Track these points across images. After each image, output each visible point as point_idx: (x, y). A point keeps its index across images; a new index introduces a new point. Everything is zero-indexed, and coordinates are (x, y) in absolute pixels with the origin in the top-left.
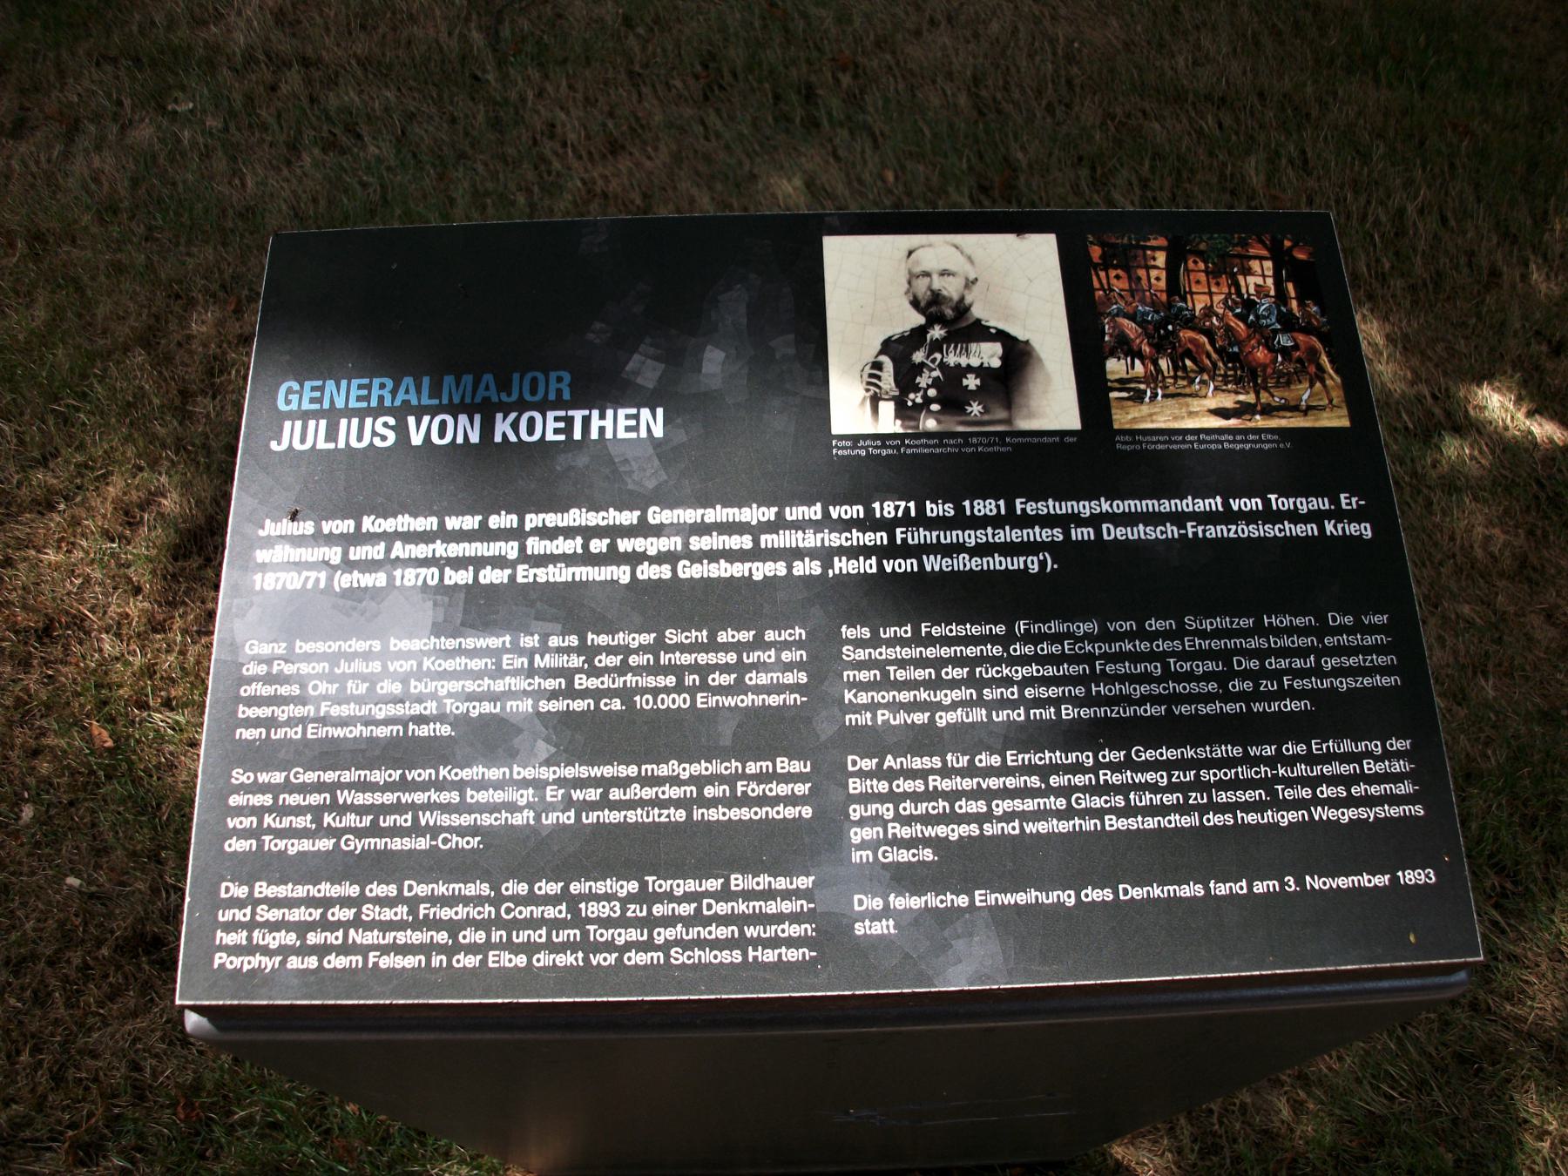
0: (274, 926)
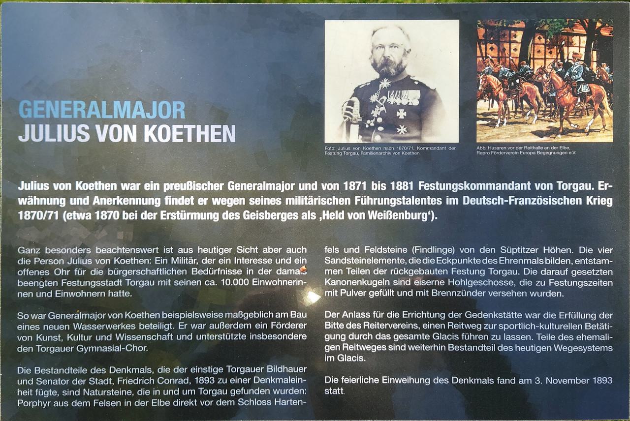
0: (46, 387)
